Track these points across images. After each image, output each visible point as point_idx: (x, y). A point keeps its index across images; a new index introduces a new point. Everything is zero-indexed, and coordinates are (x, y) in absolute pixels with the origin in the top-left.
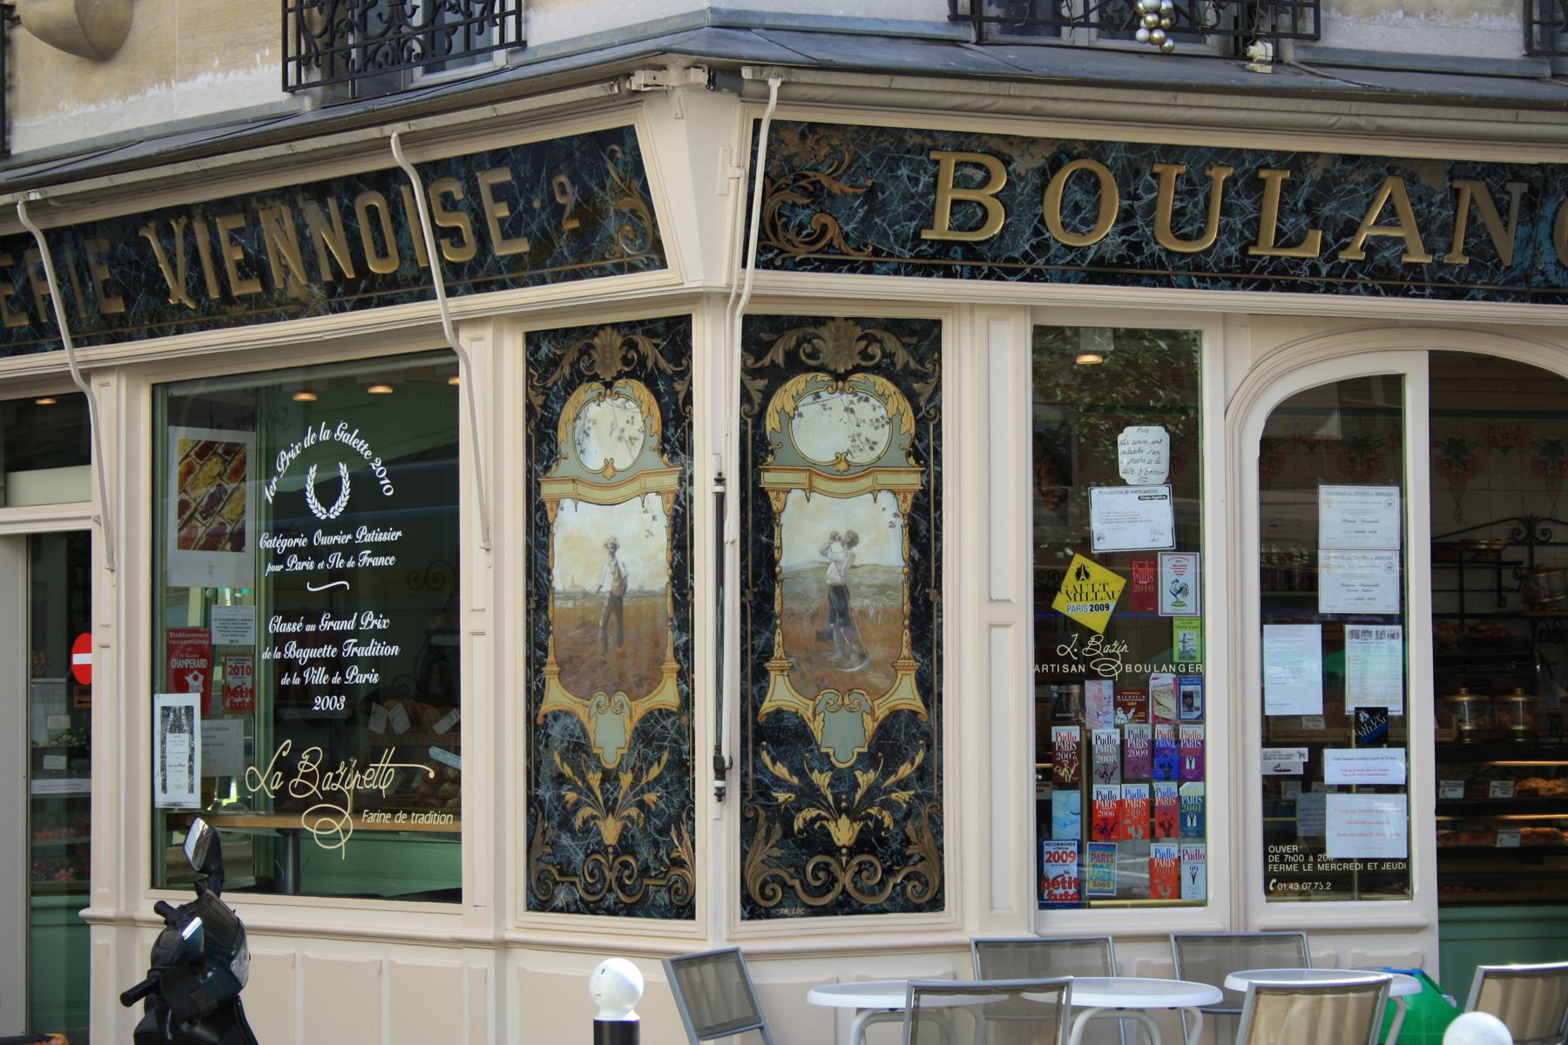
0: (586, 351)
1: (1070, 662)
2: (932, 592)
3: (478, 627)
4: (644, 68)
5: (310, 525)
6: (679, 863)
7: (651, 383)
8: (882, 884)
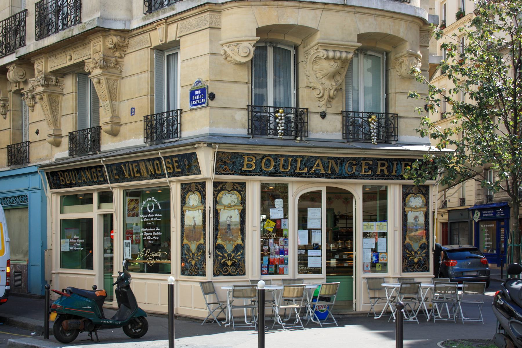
0: (190, 187)
1: (266, 236)
2: (244, 225)
3: (173, 230)
4: (197, 143)
5: (148, 213)
6: (203, 268)
7: (200, 192)
8: (236, 271)
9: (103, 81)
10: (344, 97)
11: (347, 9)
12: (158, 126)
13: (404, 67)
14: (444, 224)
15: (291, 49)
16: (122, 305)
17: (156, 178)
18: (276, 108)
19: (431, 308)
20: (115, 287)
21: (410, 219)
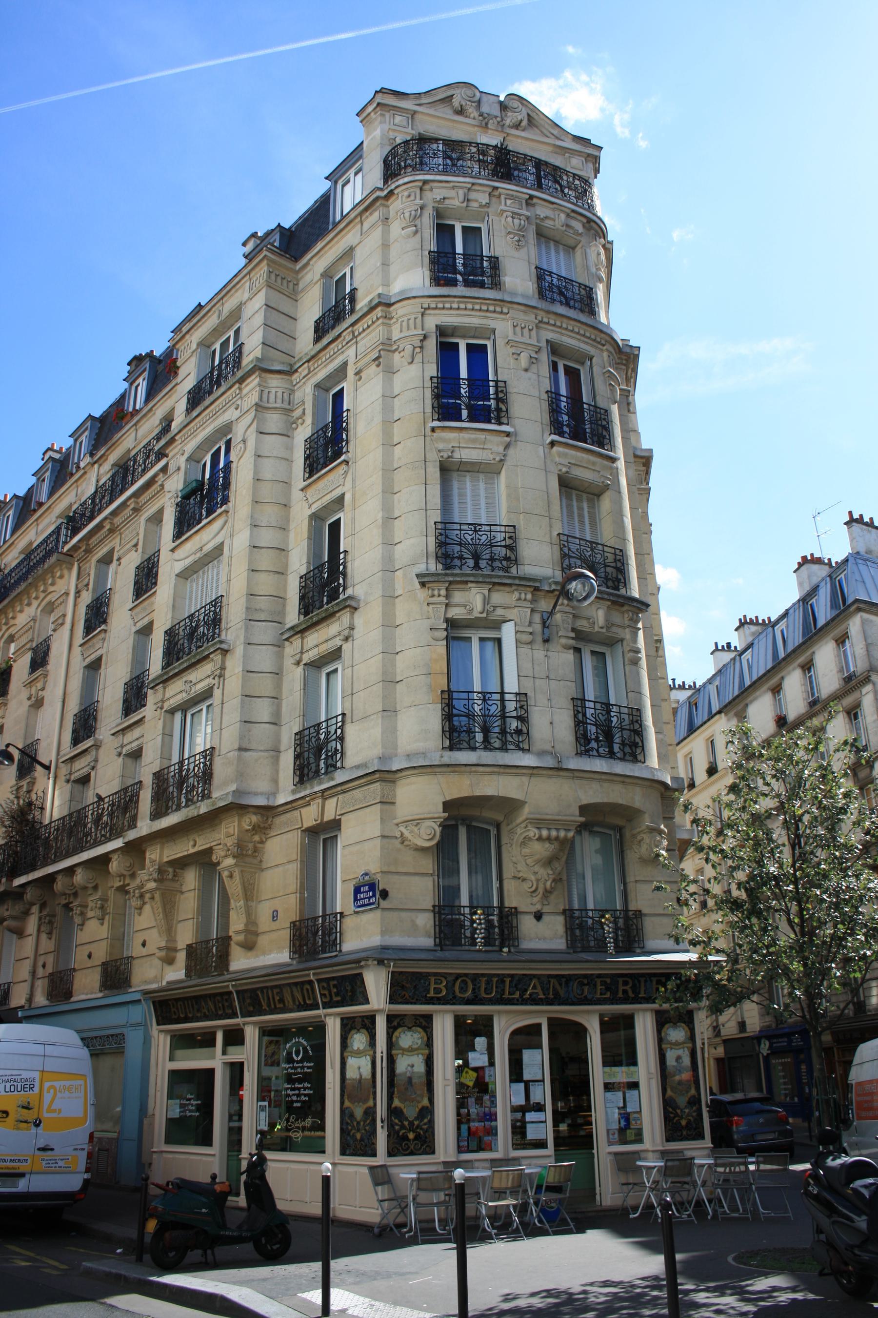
0: (354, 1022)
9: (237, 874)
10: (566, 890)
11: (562, 773)
12: (310, 935)
13: (644, 847)
14: (719, 1061)
15: (491, 828)
16: (253, 1206)
17: (305, 1010)
18: (473, 909)
19: (713, 1196)
20: (244, 1178)
21: (671, 1056)
